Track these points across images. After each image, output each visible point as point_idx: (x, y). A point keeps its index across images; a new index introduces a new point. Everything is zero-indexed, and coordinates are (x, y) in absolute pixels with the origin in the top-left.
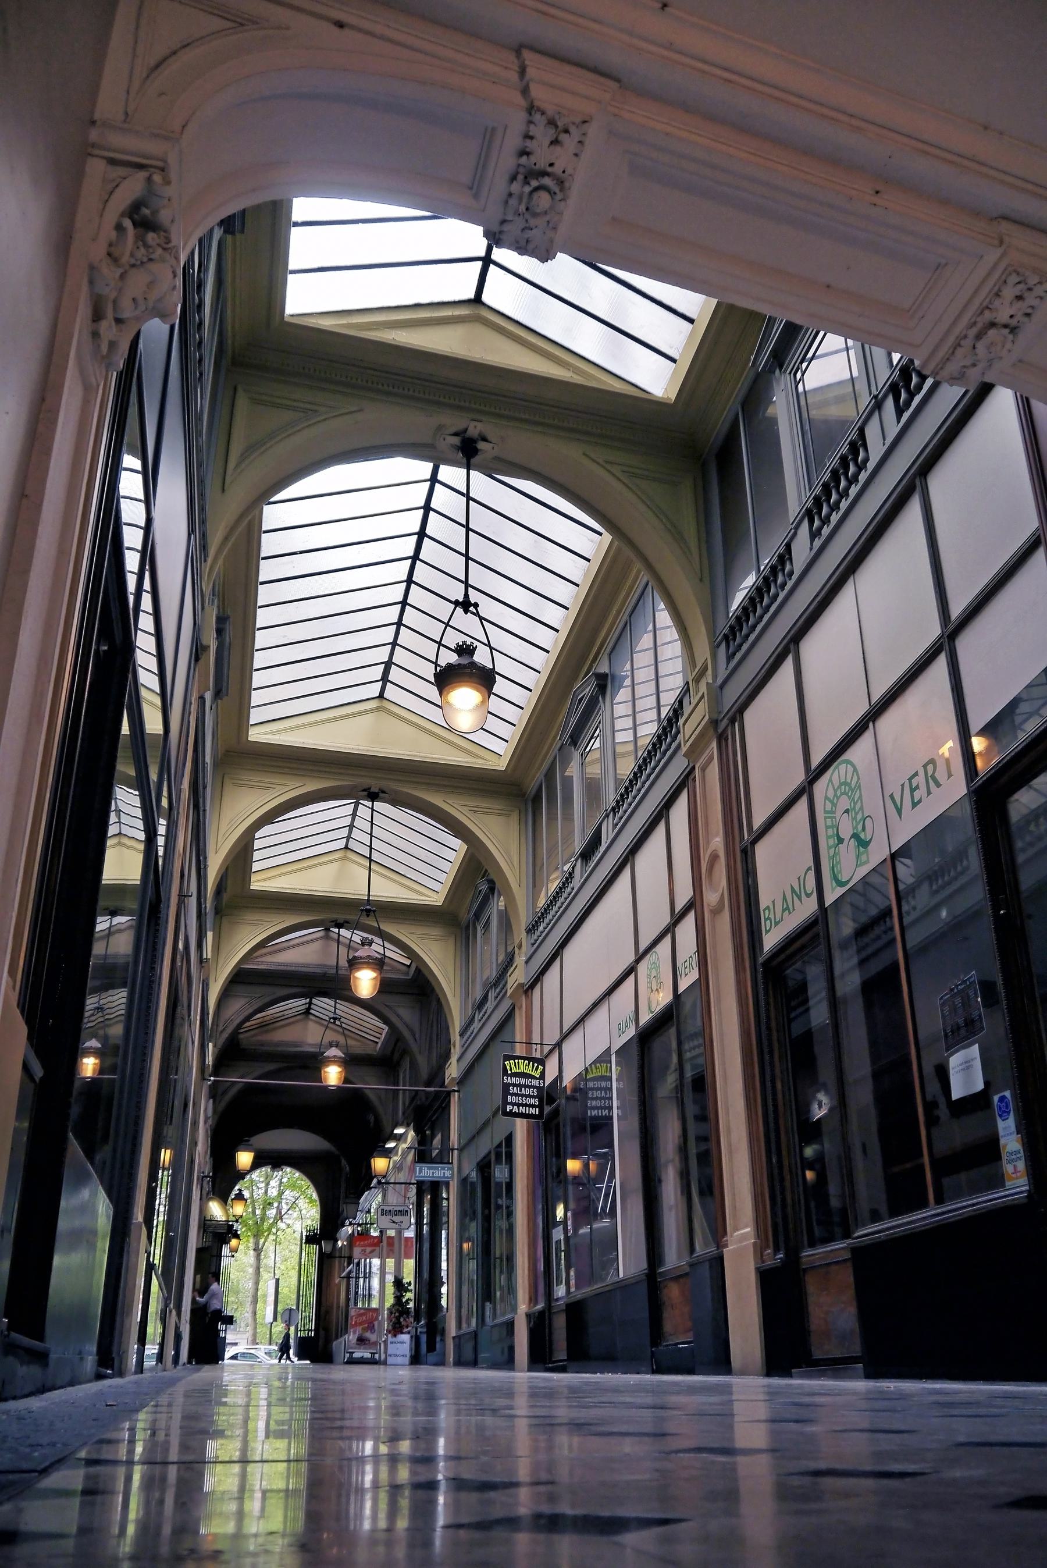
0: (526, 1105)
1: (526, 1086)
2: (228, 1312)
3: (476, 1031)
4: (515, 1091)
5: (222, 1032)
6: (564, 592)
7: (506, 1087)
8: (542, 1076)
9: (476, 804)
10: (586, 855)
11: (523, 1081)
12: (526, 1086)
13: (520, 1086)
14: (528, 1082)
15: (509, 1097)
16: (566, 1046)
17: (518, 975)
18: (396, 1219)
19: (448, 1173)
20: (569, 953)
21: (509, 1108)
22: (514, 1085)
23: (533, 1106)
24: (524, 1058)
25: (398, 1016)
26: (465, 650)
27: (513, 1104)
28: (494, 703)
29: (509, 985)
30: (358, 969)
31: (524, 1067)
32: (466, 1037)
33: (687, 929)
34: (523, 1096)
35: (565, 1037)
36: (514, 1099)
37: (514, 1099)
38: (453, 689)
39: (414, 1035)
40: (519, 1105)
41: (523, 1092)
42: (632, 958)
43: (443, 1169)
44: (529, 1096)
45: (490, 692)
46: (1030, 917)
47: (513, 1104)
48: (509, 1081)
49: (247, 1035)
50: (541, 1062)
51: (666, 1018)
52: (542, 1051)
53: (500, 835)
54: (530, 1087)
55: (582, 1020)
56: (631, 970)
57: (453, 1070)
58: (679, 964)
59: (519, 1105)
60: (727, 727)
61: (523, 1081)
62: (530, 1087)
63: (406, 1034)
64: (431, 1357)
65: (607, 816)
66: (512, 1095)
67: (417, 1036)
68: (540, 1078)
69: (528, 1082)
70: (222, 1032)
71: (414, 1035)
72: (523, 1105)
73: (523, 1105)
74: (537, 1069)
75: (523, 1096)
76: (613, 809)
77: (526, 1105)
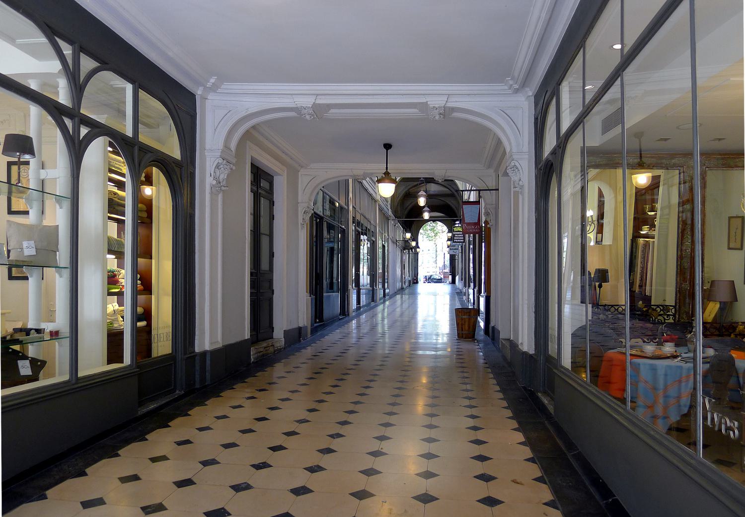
13: (458, 234)
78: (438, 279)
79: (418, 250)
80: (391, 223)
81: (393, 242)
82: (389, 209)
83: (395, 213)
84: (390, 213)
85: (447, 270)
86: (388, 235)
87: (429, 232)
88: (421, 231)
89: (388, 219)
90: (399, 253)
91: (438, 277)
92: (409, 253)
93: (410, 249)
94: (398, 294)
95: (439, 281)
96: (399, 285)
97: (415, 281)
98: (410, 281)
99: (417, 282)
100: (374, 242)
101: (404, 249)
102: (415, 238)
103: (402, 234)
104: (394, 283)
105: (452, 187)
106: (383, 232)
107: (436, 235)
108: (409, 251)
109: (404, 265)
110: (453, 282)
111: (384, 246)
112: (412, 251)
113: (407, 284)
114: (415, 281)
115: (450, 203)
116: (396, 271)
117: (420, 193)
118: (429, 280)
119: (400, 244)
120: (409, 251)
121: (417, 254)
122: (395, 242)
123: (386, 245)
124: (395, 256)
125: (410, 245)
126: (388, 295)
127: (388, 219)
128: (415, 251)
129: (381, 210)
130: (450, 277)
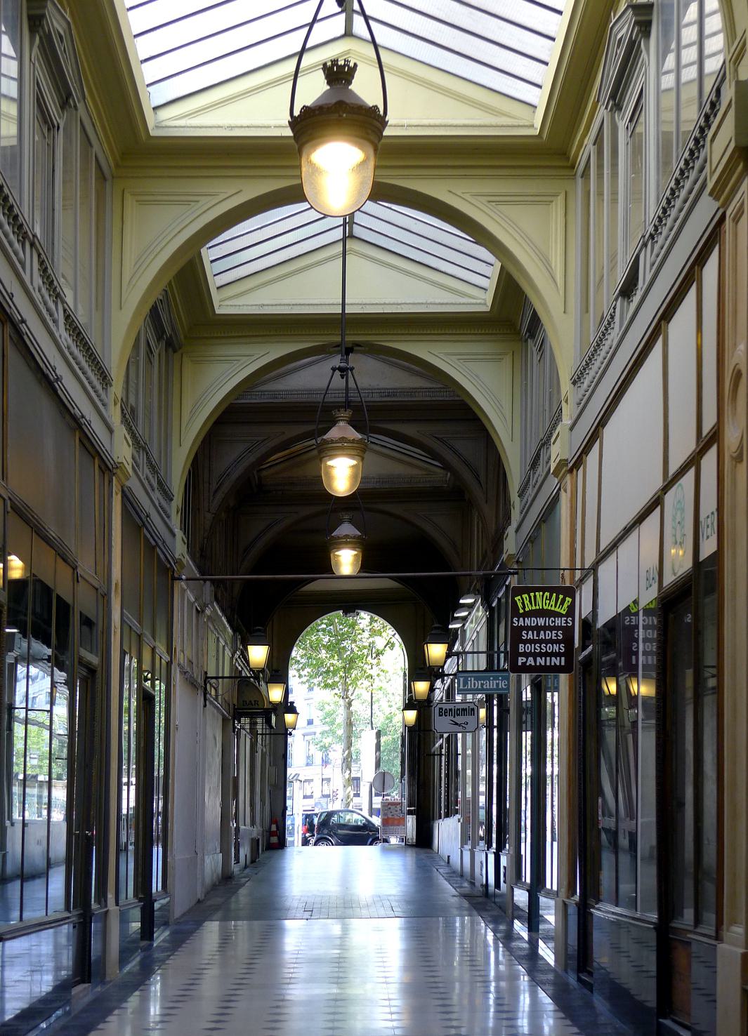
0: (546, 654)
1: (545, 628)
2: (328, 766)
4: (530, 636)
5: (216, 492)
7: (517, 632)
8: (571, 612)
9: (504, 191)
10: (627, 290)
11: (541, 621)
13: (538, 629)
14: (549, 621)
16: (602, 569)
17: (560, 450)
18: (459, 719)
19: (502, 684)
20: (608, 431)
21: (521, 660)
22: (528, 628)
24: (543, 590)
25: (455, 452)
26: (339, 74)
27: (526, 655)
29: (553, 459)
31: (543, 601)
33: (709, 462)
34: (541, 642)
35: (602, 557)
36: (529, 648)
37: (529, 648)
38: (315, 147)
39: (477, 478)
40: (535, 655)
41: (542, 636)
42: (659, 483)
43: (496, 678)
44: (552, 642)
47: (526, 655)
48: (521, 623)
49: (272, 470)
50: (570, 592)
52: (573, 576)
54: (551, 629)
55: (614, 546)
56: (657, 502)
57: (511, 545)
58: (702, 518)
59: (535, 655)
60: (216, 690)
61: (541, 621)
62: (551, 629)
63: (467, 475)
65: (645, 245)
66: (525, 642)
67: (482, 479)
68: (567, 615)
69: (549, 621)
70: (216, 492)
71: (477, 478)
72: (541, 655)
73: (541, 655)
74: (562, 603)
75: (541, 642)
76: (652, 237)
77: (546, 654)
78: (357, 828)
79: (289, 718)
80: (184, 596)
81: (192, 684)
82: (178, 531)
83: (201, 554)
84: (179, 548)
85: (396, 794)
86: (170, 649)
87: (323, 654)
88: (296, 653)
89: (167, 573)
90: (214, 731)
91: (354, 819)
92: (253, 732)
93: (257, 719)
94: (207, 917)
95: (361, 835)
96: (212, 863)
97: (274, 840)
98: (255, 843)
99: (281, 845)
100: (92, 671)
101: (237, 714)
102: (277, 671)
103: (228, 653)
104: (194, 862)
105: (451, 448)
106: (147, 633)
107: (350, 664)
108: (253, 724)
109: (236, 780)
110: (424, 839)
111: (147, 700)
112: (268, 721)
113: (245, 851)
114: (274, 840)
115: (428, 528)
116: (196, 847)
117: (334, 433)
118: (326, 830)
119: (223, 689)
120: (253, 724)
121: (283, 733)
122: (201, 685)
123: (160, 698)
124: (194, 734)
125: (262, 697)
126: (166, 924)
127: (167, 573)
128: (281, 721)
129: (135, 521)
130: (411, 822)
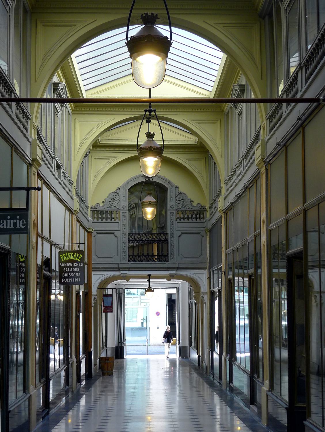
1: (72, 267)
3: (284, 115)
4: (67, 270)
6: (217, 67)
11: (71, 265)
12: (72, 267)
13: (69, 267)
15: (63, 274)
22: (66, 267)
23: (77, 272)
28: (169, 61)
30: (145, 156)
32: (229, 185)
45: (167, 56)
46: (64, 376)
47: (65, 278)
51: (37, 425)
53: (209, 132)
61: (71, 265)
64: (129, 259)
66: (65, 273)
69: (74, 264)
74: (78, 257)
